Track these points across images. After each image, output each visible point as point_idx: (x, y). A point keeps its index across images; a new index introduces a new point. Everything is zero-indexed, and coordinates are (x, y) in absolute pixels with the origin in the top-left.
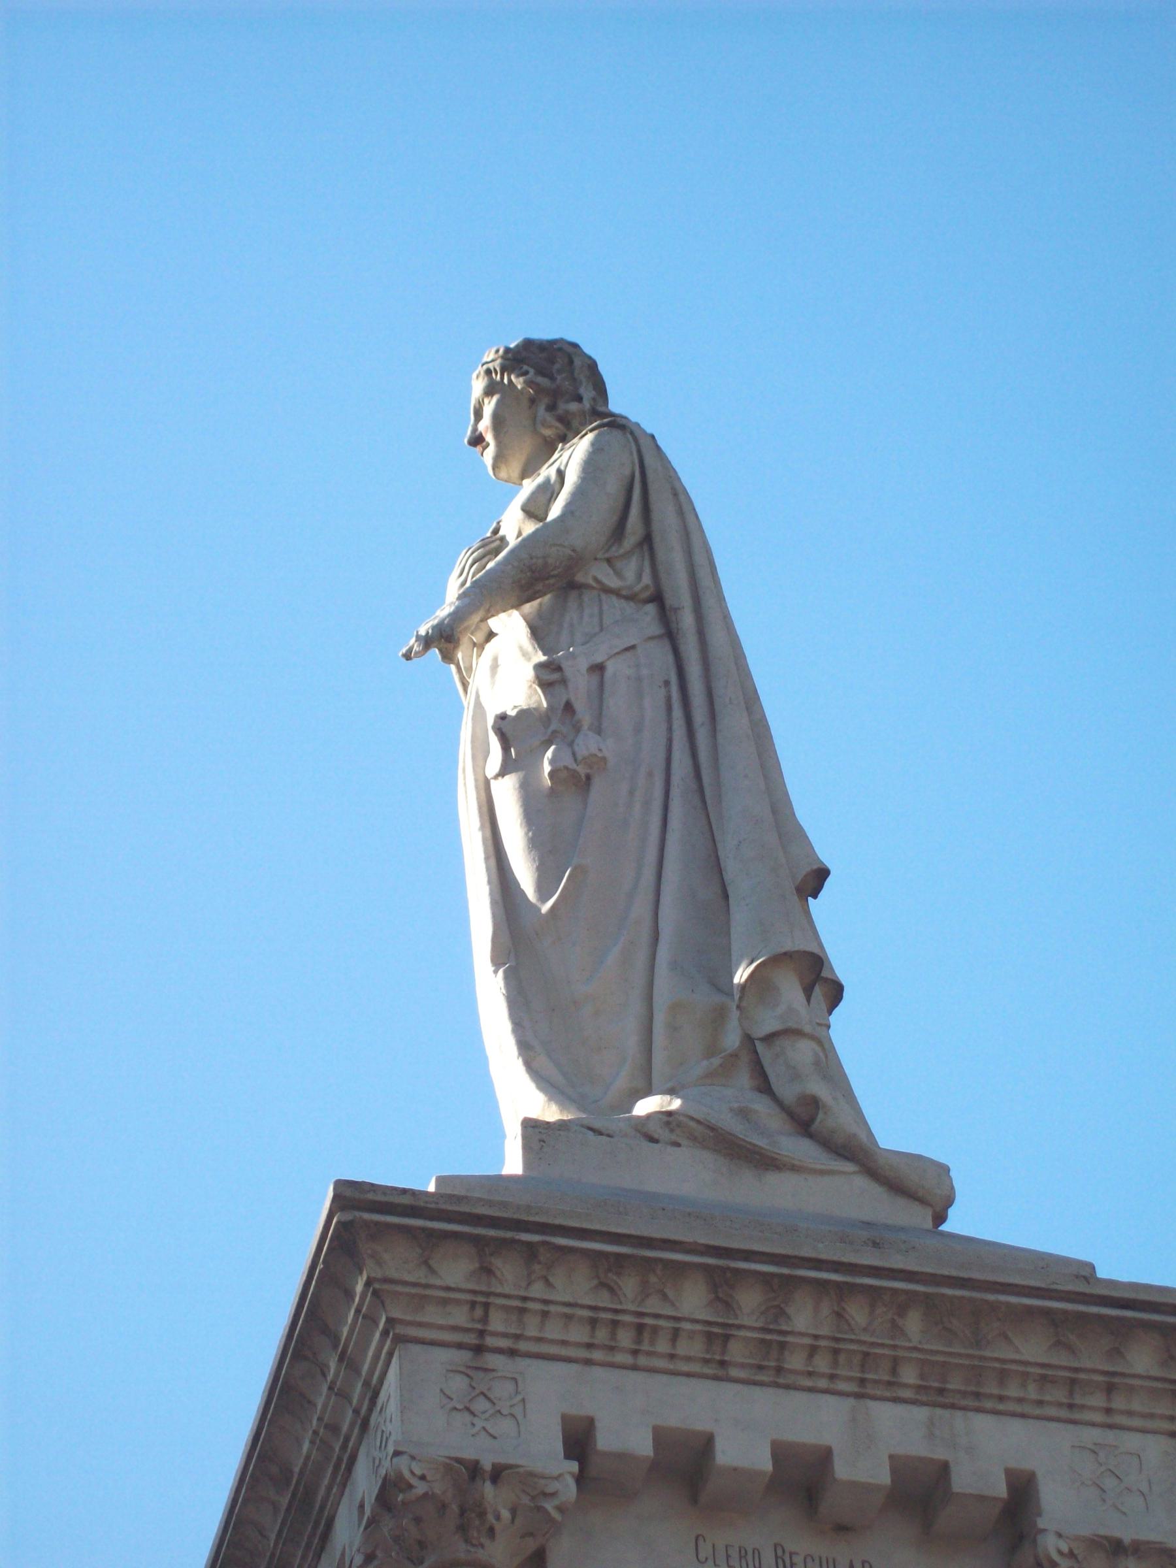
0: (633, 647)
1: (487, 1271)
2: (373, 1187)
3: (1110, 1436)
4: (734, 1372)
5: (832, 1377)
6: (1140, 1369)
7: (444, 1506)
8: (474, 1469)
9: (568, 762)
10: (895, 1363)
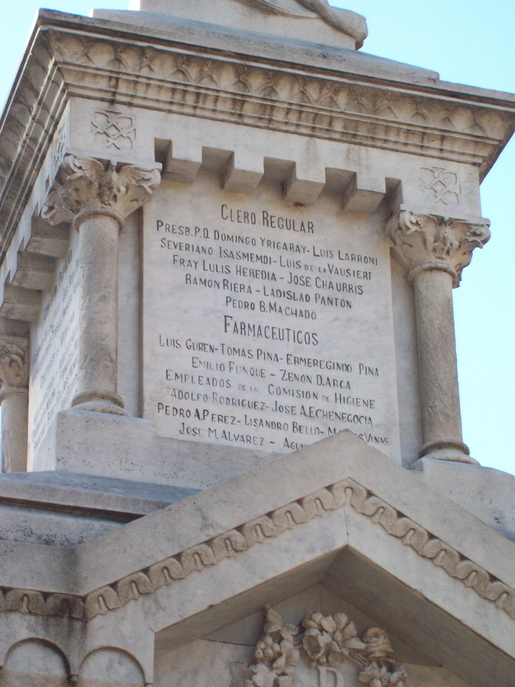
1: (119, 61)
2: (60, 13)
3: (441, 164)
4: (246, 121)
5: (195, 107)
8: (107, 165)
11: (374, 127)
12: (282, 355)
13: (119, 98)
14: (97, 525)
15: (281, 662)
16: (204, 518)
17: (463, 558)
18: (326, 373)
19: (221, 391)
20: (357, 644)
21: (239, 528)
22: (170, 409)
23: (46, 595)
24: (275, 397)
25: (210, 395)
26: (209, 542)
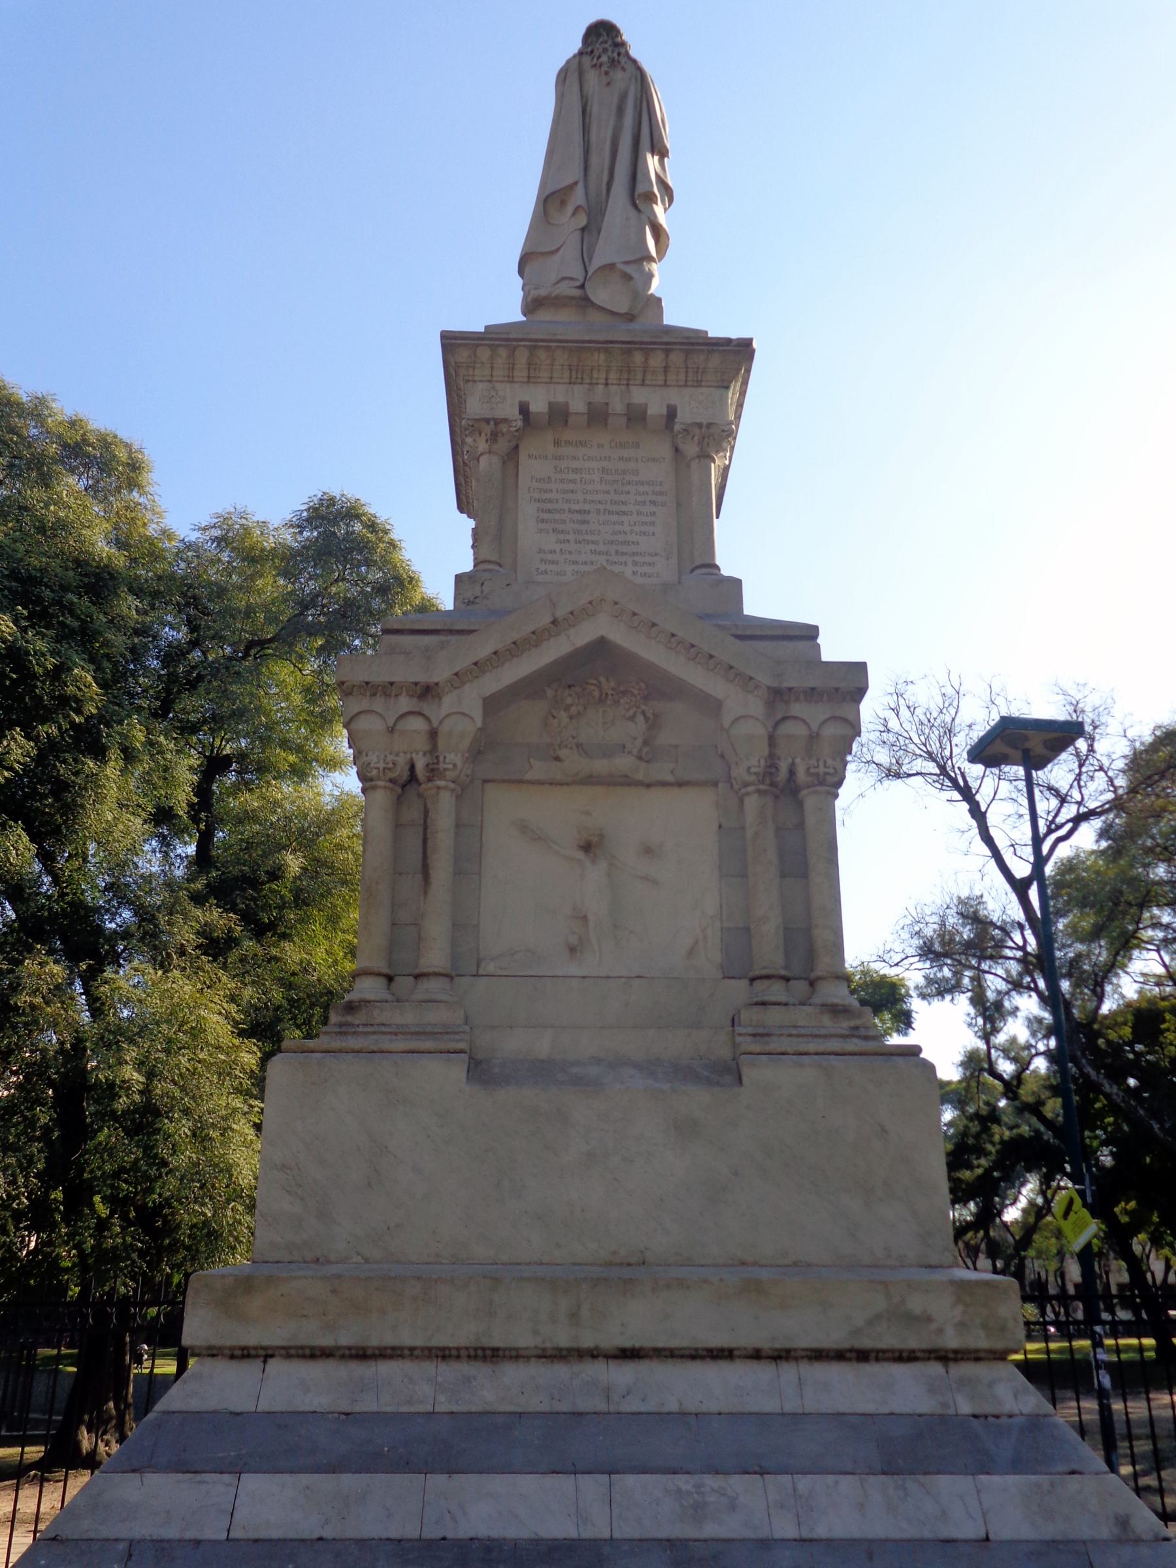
23: (416, 684)
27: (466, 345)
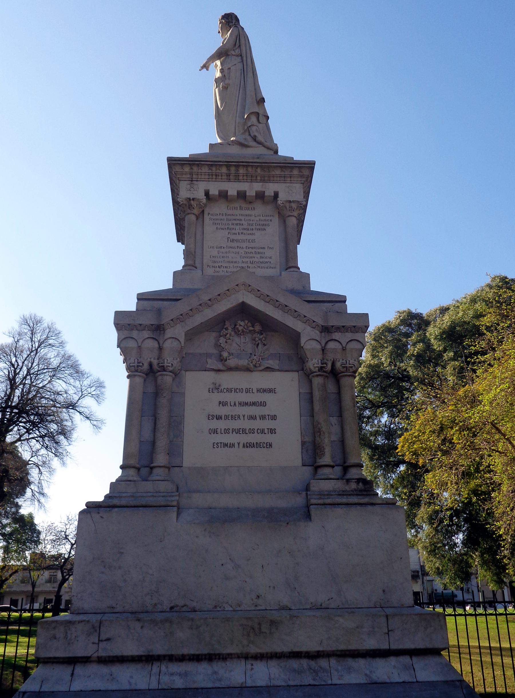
0: (235, 64)
1: (192, 169)
2: (173, 157)
3: (291, 184)
4: (231, 180)
5: (216, 179)
6: (295, 174)
7: (186, 205)
8: (190, 199)
9: (224, 85)
10: (256, 177)
11: (269, 177)
12: (244, 247)
13: (193, 179)
14: (165, 303)
15: (228, 335)
16: (199, 298)
17: (277, 301)
18: (257, 250)
19: (226, 260)
20: (251, 328)
21: (210, 300)
22: (211, 267)
23: (152, 325)
24: (242, 259)
25: (223, 261)
26: (200, 305)
27: (296, 167)
